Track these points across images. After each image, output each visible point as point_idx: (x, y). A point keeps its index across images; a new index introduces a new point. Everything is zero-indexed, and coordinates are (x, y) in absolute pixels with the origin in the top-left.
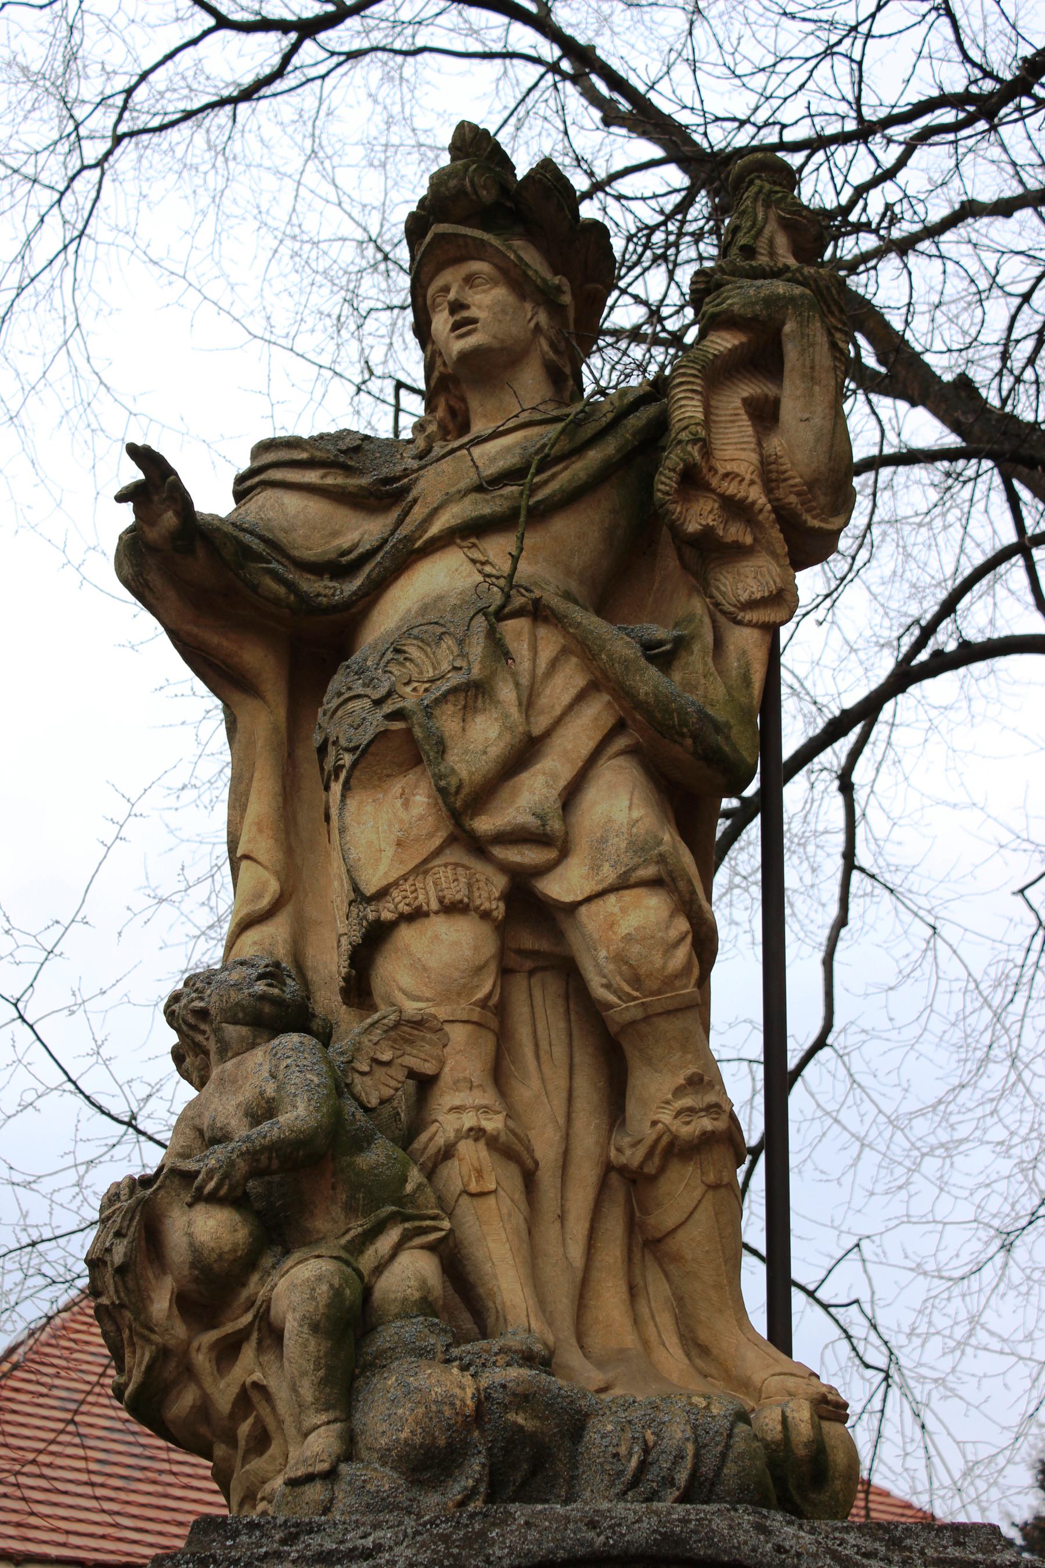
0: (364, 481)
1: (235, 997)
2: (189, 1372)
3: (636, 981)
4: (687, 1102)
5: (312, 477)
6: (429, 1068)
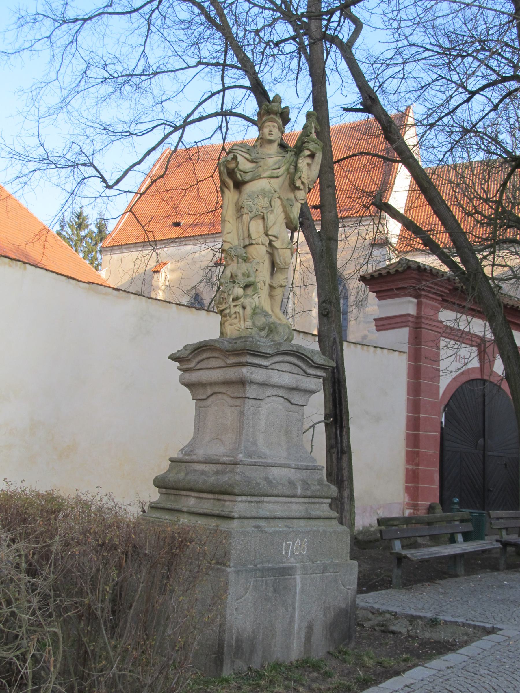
2: (230, 308)
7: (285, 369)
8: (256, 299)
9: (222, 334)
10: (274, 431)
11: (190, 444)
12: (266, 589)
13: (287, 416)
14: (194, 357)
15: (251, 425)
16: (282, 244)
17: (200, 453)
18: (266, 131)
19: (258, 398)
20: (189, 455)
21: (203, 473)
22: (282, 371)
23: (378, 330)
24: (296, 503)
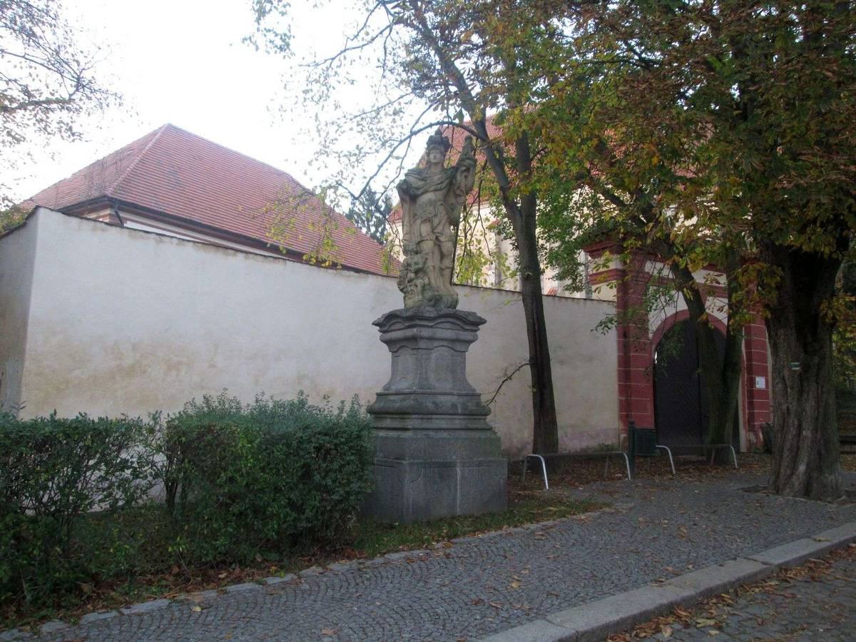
11: (389, 383)
17: (394, 388)
21: (394, 401)
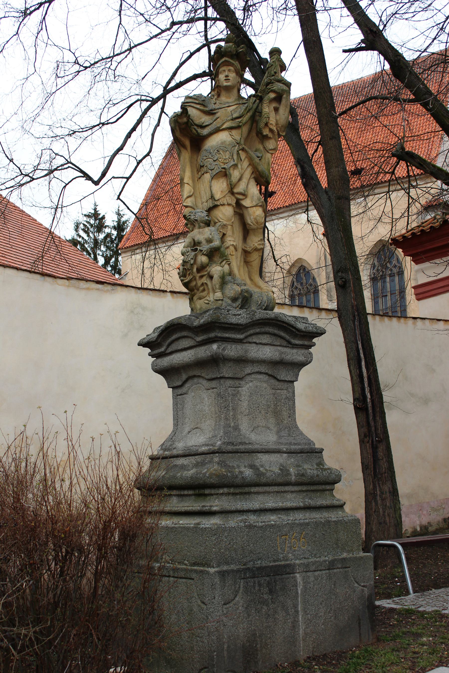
0: (207, 109)
1: (203, 219)
2: (195, 279)
3: (257, 223)
4: (260, 243)
5: (198, 106)
6: (225, 233)
7: (264, 342)
8: (227, 267)
9: (192, 310)
10: (260, 412)
12: (260, 590)
13: (274, 394)
14: (164, 339)
15: (231, 408)
16: (252, 202)
17: (180, 446)
18: (222, 77)
19: (236, 376)
20: (169, 450)
21: (183, 467)
22: (261, 344)
23: (418, 299)
24: (292, 492)
